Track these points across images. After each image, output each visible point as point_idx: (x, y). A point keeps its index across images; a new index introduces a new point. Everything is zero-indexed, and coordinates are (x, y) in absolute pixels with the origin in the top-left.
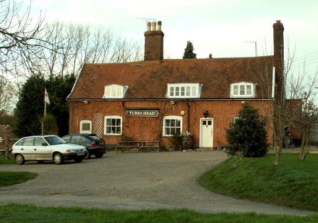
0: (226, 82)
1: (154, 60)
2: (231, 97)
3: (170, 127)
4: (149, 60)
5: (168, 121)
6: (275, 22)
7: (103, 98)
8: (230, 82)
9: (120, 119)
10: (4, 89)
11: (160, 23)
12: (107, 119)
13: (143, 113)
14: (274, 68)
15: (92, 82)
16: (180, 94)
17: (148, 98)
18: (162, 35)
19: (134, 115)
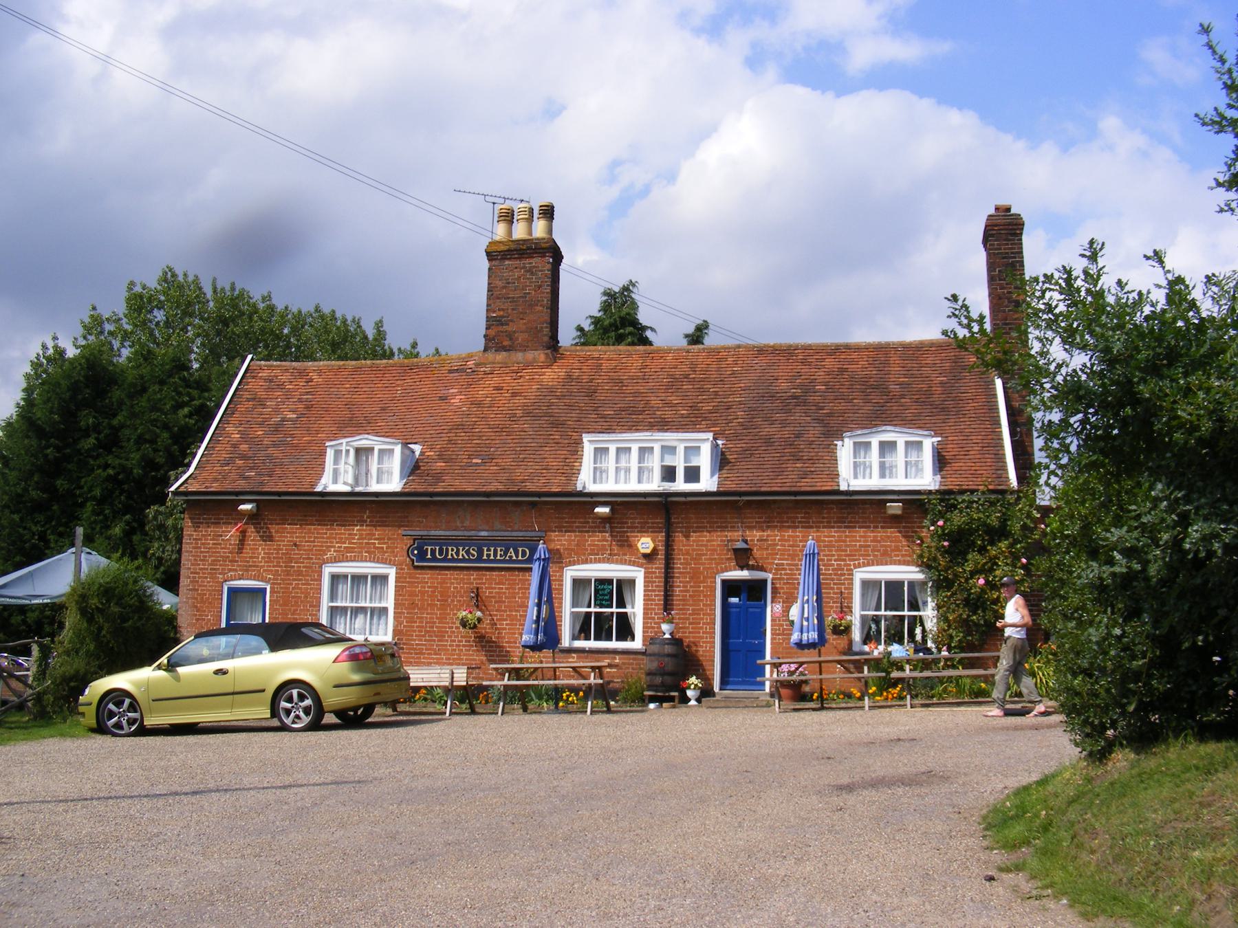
0: (814, 431)
1: (524, 348)
2: (843, 487)
3: (906, 613)
4: (505, 349)
5: (579, 584)
6: (992, 211)
7: (319, 489)
8: (833, 433)
9: (632, 582)
10: (159, 440)
11: (548, 212)
12: (866, 584)
13: (480, 552)
14: (999, 383)
15: (277, 429)
16: (680, 474)
17: (501, 488)
18: (557, 255)
19: (445, 560)
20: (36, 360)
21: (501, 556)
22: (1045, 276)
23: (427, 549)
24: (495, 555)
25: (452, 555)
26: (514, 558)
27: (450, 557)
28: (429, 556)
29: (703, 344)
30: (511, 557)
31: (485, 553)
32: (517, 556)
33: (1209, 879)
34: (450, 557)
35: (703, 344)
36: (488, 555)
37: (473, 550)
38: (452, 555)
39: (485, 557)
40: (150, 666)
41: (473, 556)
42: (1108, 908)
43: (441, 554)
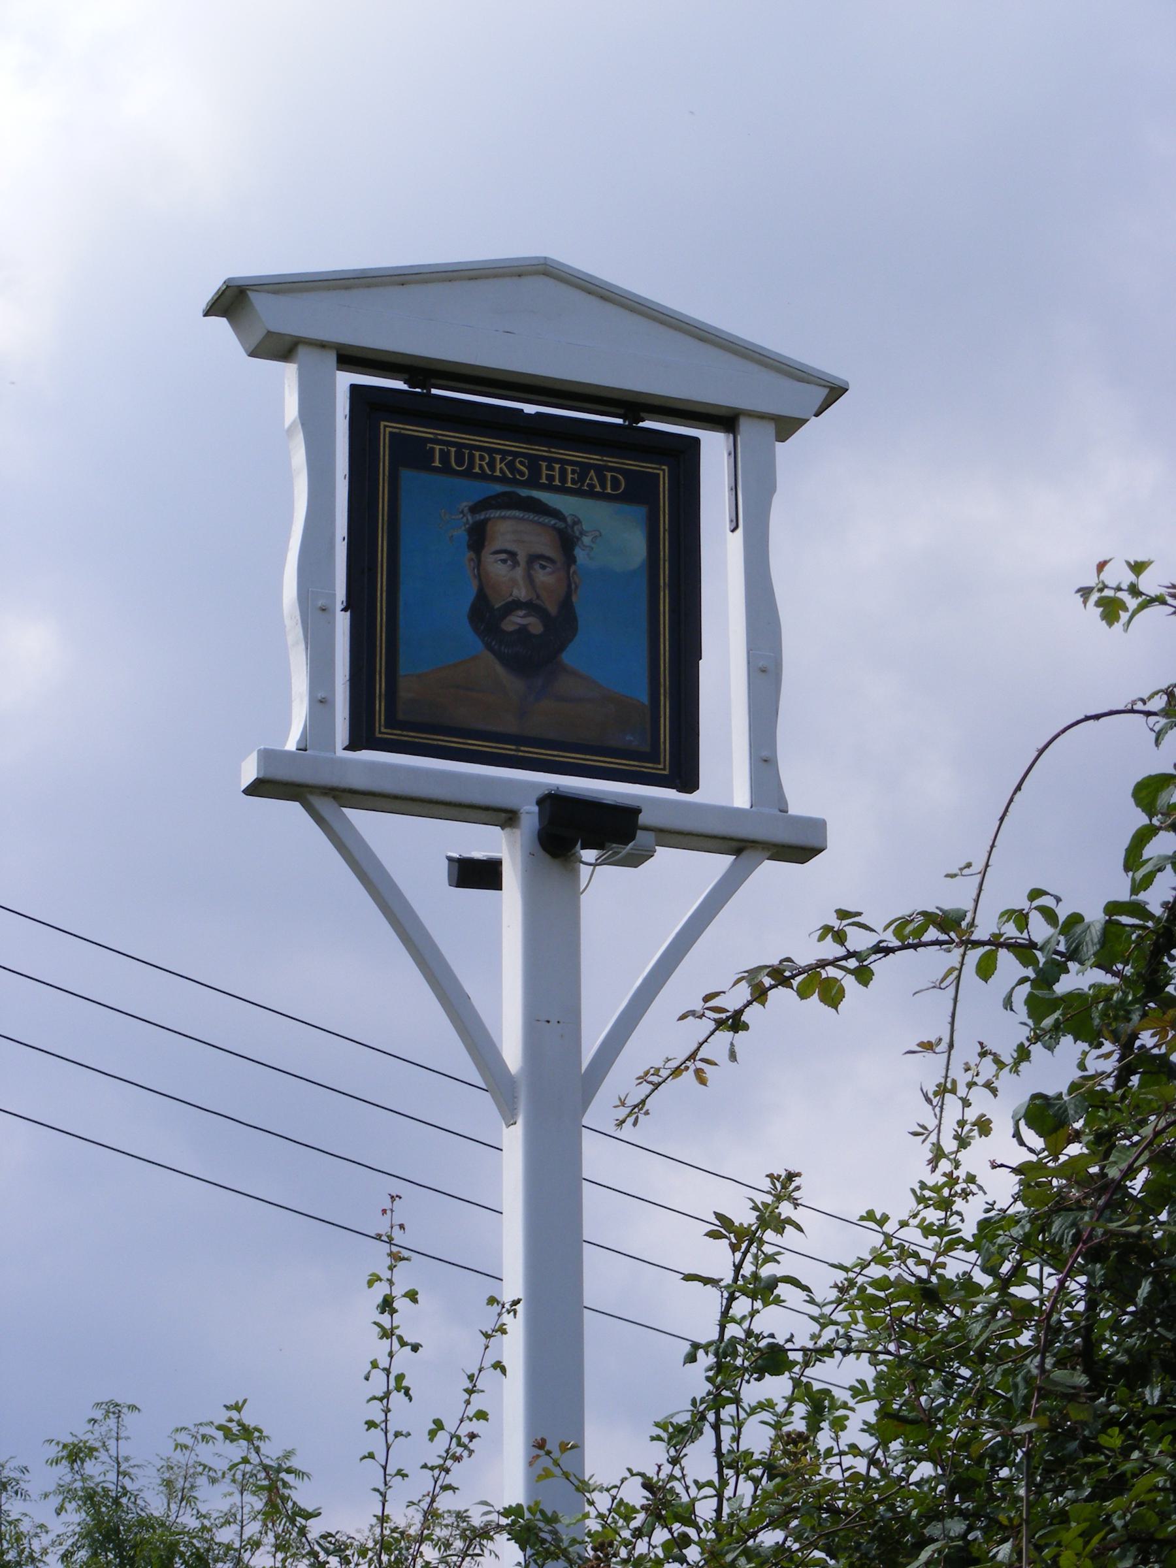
20: (509, 562)
21: (573, 481)
22: (395, 1266)
23: (433, 449)
24: (563, 478)
25: (481, 467)
26: (598, 489)
27: (477, 470)
28: (437, 464)
29: (966, 912)
30: (592, 486)
31: (545, 472)
32: (603, 486)
33: (82, 1475)
34: (477, 470)
35: (966, 912)
36: (551, 478)
37: (521, 463)
38: (481, 467)
39: (544, 481)
40: (1064, 922)
41: (522, 474)
42: (1044, 1317)
43: (460, 462)
